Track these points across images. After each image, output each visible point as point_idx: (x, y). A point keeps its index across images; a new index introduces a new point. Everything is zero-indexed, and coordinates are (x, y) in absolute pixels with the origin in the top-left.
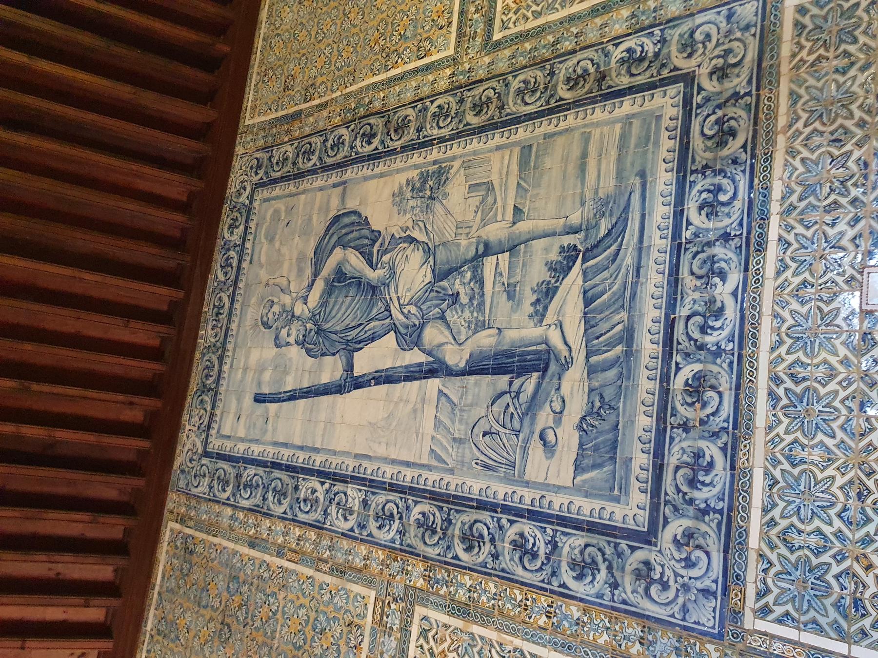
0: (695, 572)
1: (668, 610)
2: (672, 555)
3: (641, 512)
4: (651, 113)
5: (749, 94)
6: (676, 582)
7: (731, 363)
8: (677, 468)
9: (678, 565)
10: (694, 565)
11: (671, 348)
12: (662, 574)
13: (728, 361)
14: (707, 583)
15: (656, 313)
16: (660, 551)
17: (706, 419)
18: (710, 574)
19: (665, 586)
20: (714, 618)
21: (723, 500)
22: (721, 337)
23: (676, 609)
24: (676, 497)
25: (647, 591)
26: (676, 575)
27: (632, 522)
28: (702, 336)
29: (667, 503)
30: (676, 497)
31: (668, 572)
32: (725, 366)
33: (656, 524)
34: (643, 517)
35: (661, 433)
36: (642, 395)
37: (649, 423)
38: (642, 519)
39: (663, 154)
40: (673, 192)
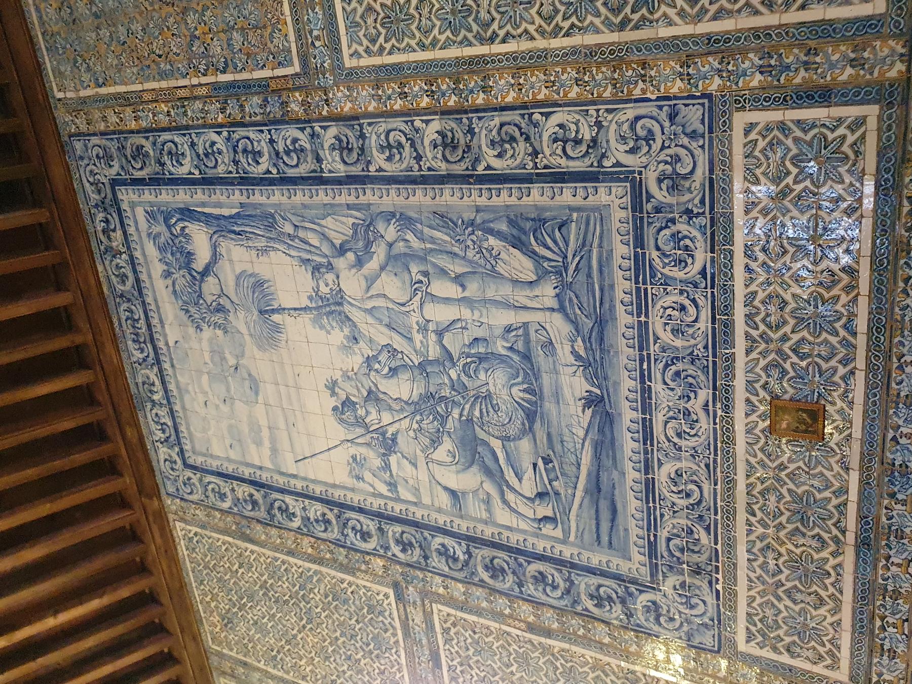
0: (657, 129)
1: (698, 152)
2: (645, 154)
3: (614, 190)
4: (596, 209)
5: (118, 139)
6: (669, 147)
7: (607, 110)
8: (569, 157)
9: (654, 147)
10: (650, 131)
11: (471, 176)
12: (666, 163)
13: (605, 115)
14: (663, 115)
15: (419, 193)
16: (645, 167)
17: (524, 136)
18: (655, 114)
19: (677, 159)
20: (694, 105)
21: (587, 111)
22: (459, 131)
23: (694, 144)
24: (592, 156)
25: (685, 177)
26: (663, 148)
27: (624, 200)
28: (584, 142)
29: (600, 165)
30: (468, 160)
31: (662, 157)
32: (610, 117)
33: (621, 175)
34: (619, 189)
35: (423, 180)
36: (545, 201)
37: (536, 190)
38: (620, 189)
39: (284, 199)
40: (459, 186)
